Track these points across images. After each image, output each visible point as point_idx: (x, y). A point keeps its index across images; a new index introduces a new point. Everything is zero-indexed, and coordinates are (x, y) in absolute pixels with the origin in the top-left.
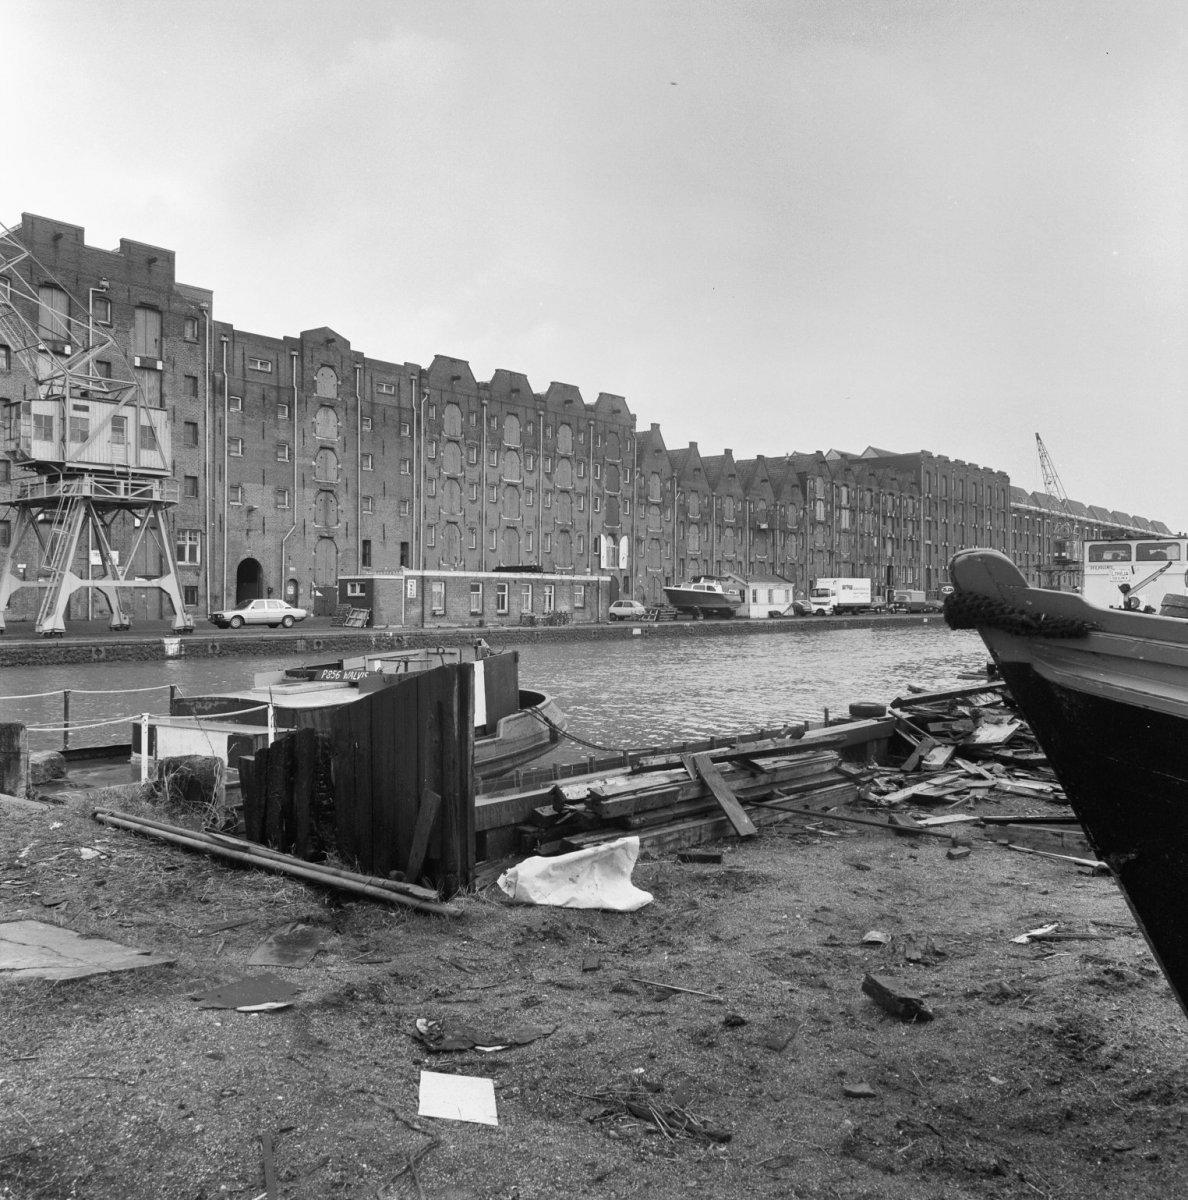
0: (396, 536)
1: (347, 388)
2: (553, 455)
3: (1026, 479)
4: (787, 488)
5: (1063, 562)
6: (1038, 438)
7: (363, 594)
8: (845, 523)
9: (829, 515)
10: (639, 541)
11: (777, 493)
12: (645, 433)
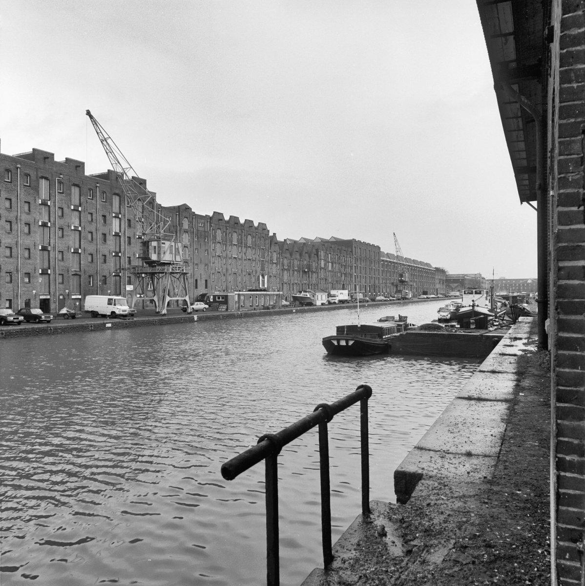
0: (204, 277)
1: (191, 225)
2: (246, 247)
3: (387, 248)
4: (313, 255)
5: (402, 282)
6: (394, 234)
7: (224, 300)
8: (330, 268)
9: (325, 265)
10: (270, 276)
11: (310, 257)
12: (272, 236)
